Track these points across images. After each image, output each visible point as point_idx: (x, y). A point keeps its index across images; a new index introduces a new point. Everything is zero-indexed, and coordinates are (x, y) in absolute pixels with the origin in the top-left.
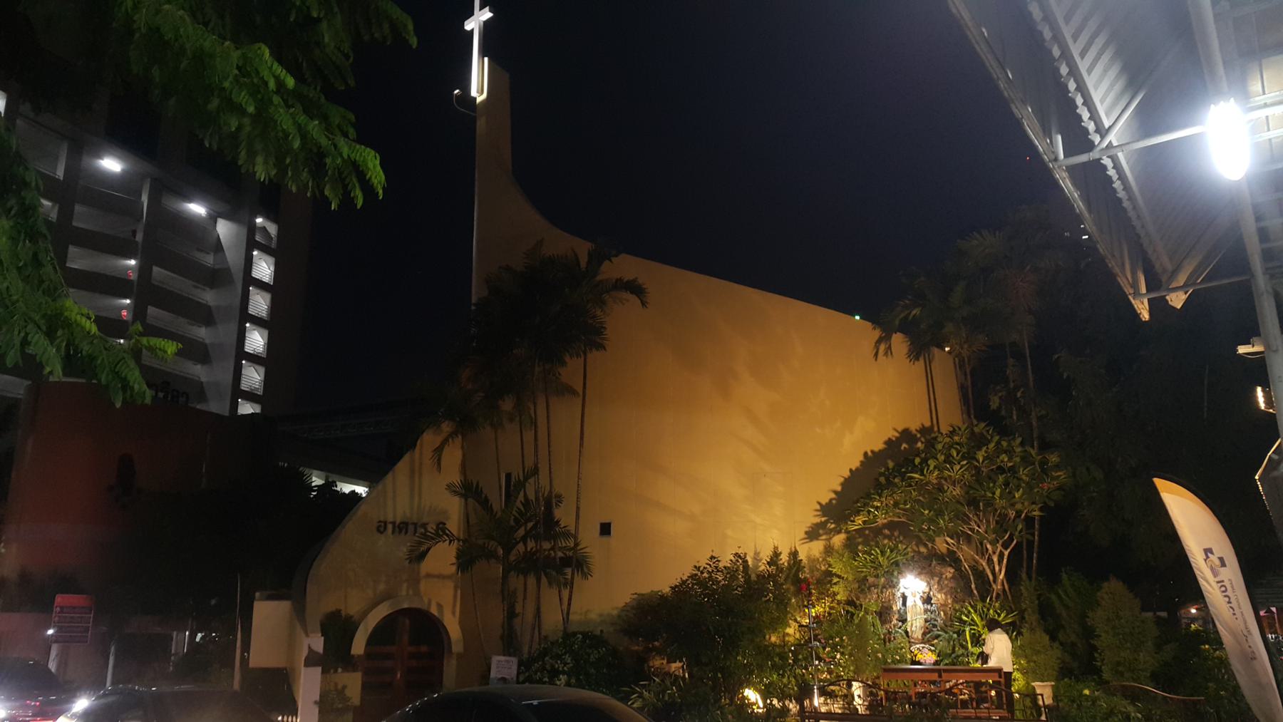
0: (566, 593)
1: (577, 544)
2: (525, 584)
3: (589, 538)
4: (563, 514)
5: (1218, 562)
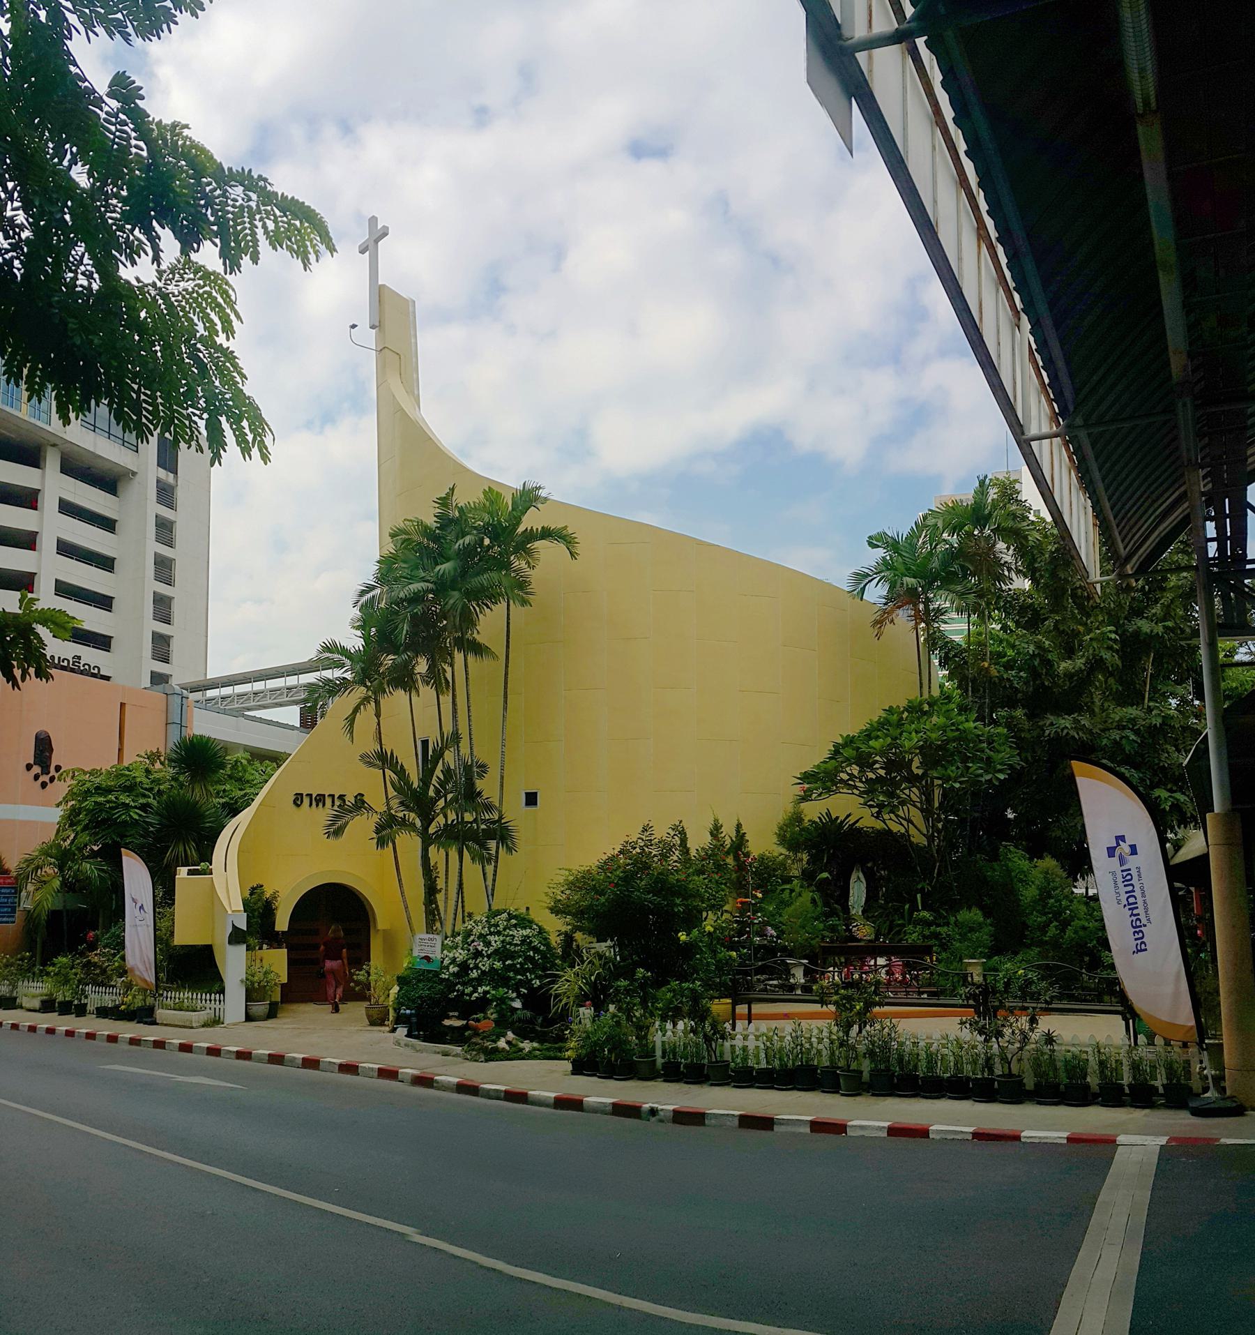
0: (490, 869)
1: (501, 818)
2: (447, 855)
3: (514, 812)
4: (486, 786)
5: (1128, 850)
